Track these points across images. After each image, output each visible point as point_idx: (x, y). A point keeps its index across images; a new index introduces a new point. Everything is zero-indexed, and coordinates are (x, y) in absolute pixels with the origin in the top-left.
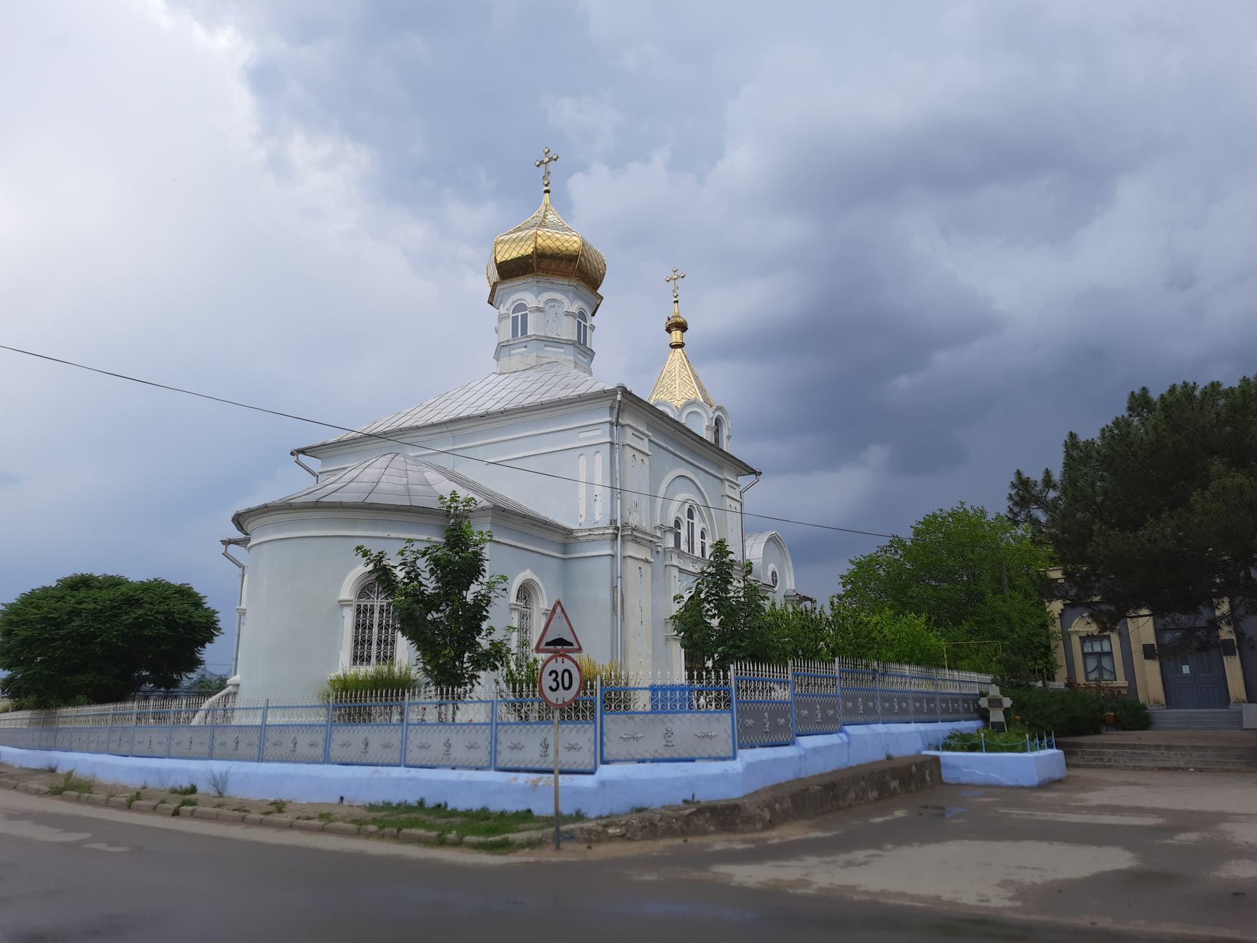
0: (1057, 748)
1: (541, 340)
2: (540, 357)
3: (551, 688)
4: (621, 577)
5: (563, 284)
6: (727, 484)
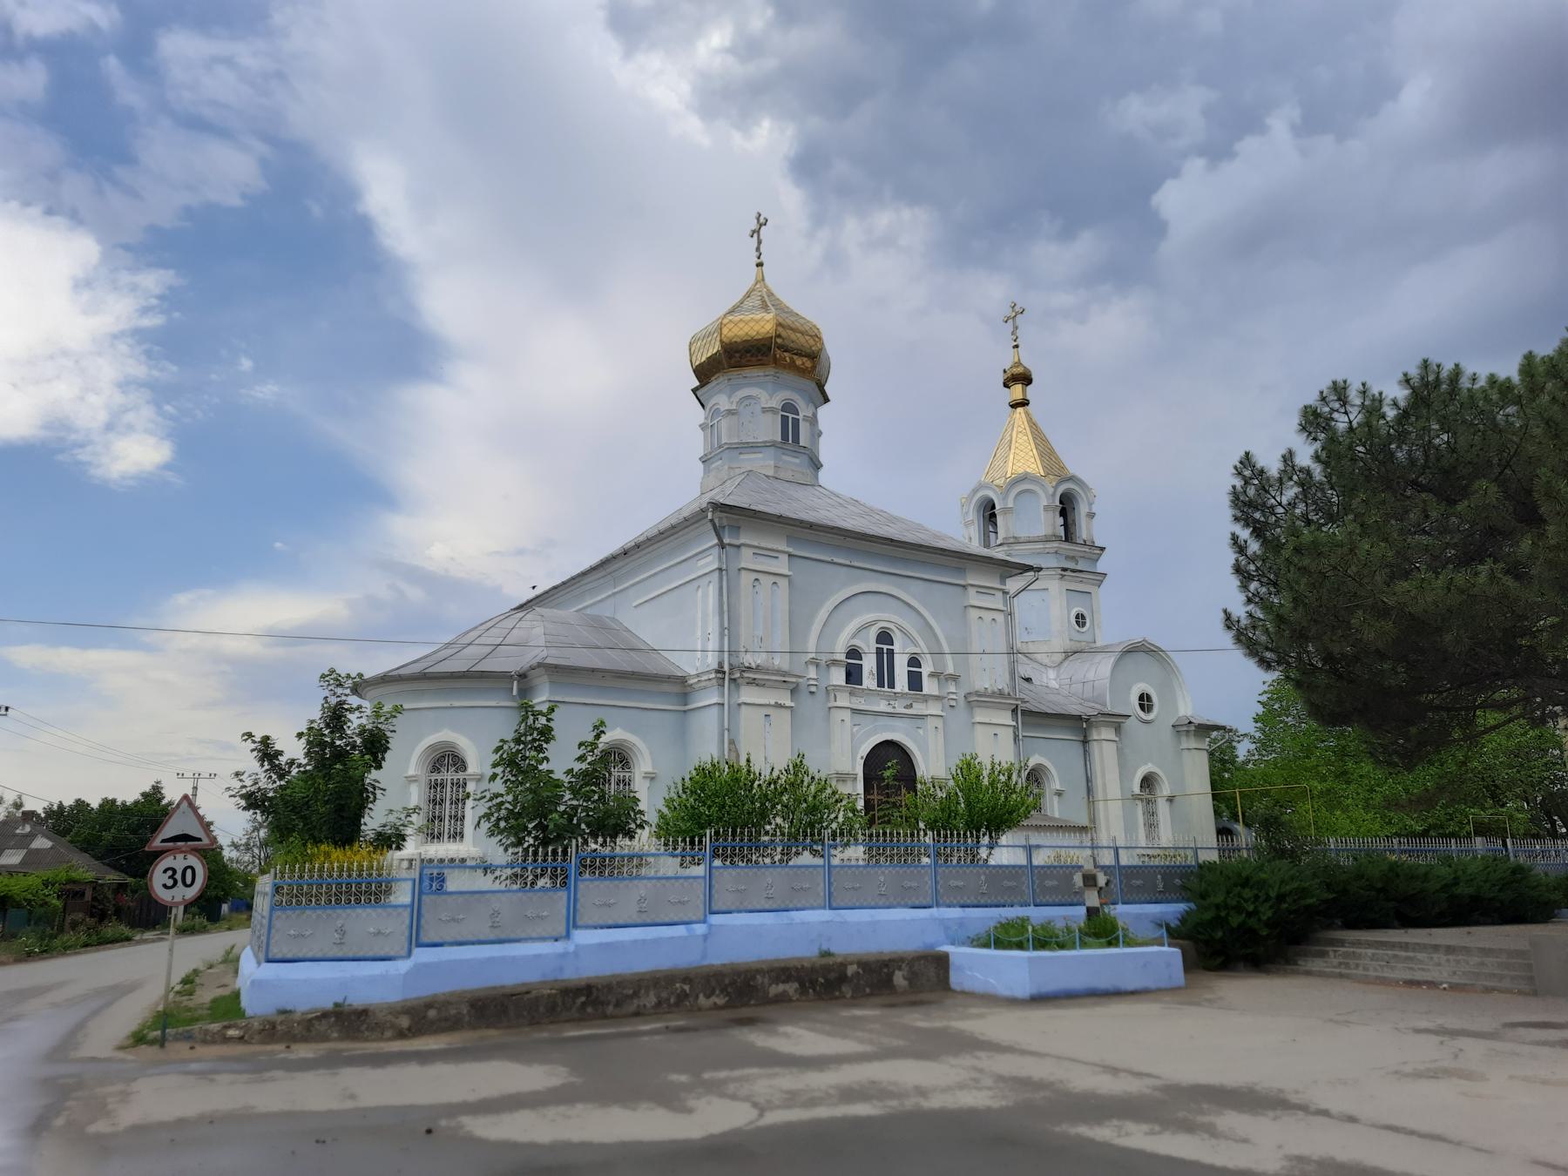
2: (732, 468)
3: (165, 886)
6: (972, 591)
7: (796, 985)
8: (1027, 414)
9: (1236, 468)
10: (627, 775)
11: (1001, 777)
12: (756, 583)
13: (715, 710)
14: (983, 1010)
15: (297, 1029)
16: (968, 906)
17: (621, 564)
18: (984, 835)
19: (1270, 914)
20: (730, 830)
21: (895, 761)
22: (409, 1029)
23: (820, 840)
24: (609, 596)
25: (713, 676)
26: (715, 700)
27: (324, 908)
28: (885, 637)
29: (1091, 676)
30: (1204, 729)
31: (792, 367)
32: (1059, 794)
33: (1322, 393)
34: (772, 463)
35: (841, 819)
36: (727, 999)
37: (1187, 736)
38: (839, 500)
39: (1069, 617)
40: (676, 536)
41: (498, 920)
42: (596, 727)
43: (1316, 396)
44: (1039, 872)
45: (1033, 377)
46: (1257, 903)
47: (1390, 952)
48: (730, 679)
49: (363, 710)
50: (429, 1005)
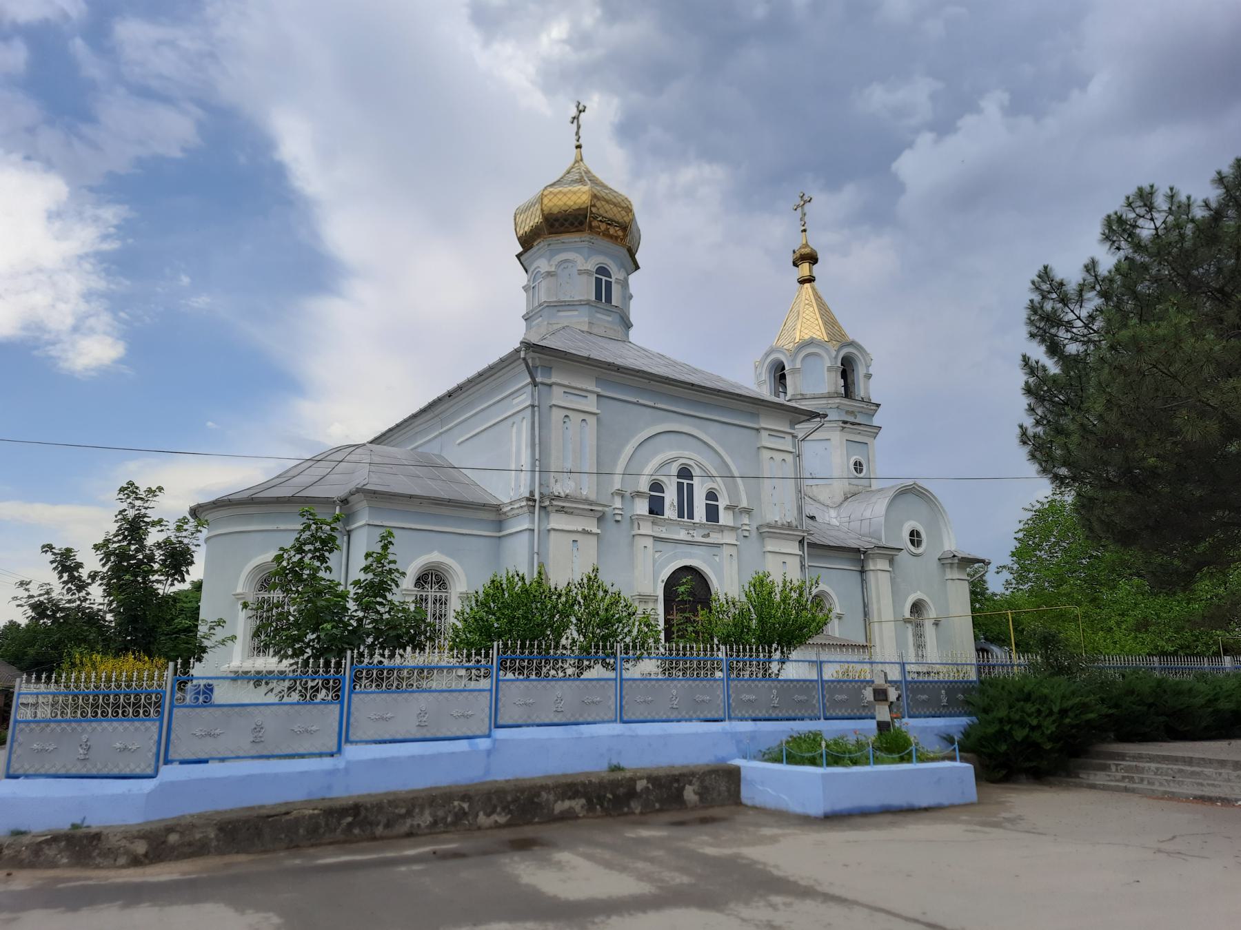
0: (961, 761)
1: (552, 306)
2: (551, 324)
4: (538, 554)
5: (575, 242)
6: (764, 434)
7: (583, 801)
8: (813, 289)
9: (1033, 283)
10: (444, 595)
11: (793, 594)
12: (566, 420)
13: (526, 535)
14: (776, 831)
15: (25, 854)
16: (760, 720)
17: (446, 406)
18: (775, 651)
19: (1053, 728)
20: (519, 642)
21: (689, 578)
22: (146, 855)
23: (612, 653)
24: (436, 437)
25: (524, 503)
26: (526, 527)
27: (132, 721)
28: (685, 473)
29: (868, 514)
30: (966, 562)
31: (606, 234)
32: (840, 617)
33: (1128, 198)
34: (587, 319)
35: (635, 632)
36: (509, 816)
37: (951, 568)
38: (645, 353)
39: (848, 464)
40: (493, 377)
41: (260, 735)
42: (383, 538)
43: (1122, 201)
44: (830, 686)
45: (819, 256)
46: (1040, 718)
47: (1175, 767)
48: (541, 507)
49: (165, 523)
50: (170, 830)
